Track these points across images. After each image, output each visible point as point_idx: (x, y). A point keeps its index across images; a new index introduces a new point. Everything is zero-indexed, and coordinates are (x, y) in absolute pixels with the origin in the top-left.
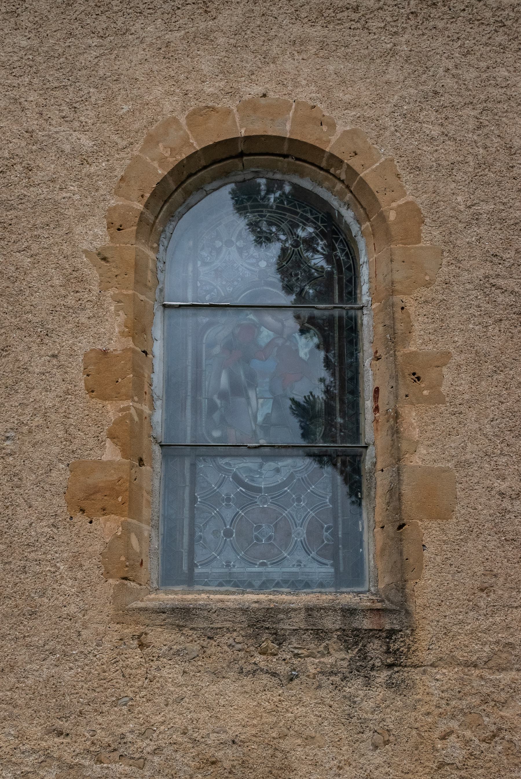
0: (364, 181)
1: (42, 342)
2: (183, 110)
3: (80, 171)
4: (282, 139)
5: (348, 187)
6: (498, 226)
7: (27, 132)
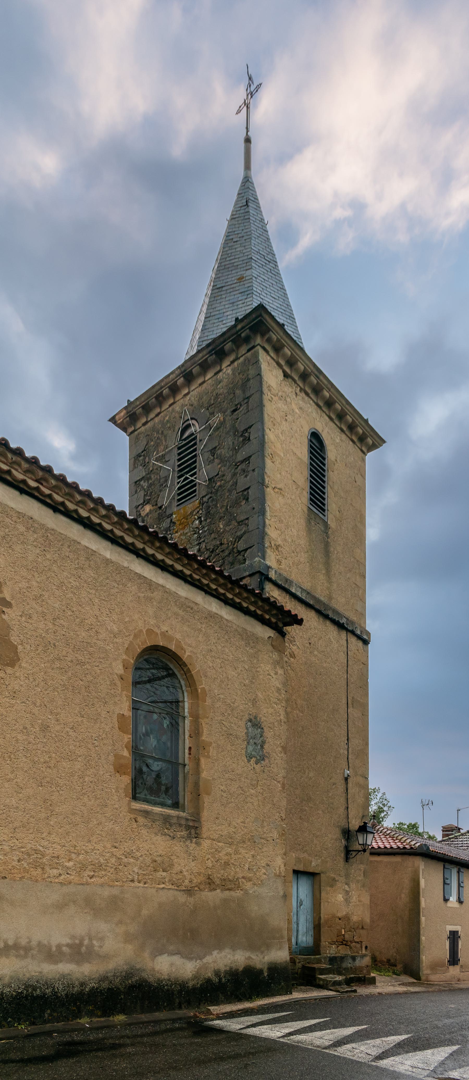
4: (171, 650)
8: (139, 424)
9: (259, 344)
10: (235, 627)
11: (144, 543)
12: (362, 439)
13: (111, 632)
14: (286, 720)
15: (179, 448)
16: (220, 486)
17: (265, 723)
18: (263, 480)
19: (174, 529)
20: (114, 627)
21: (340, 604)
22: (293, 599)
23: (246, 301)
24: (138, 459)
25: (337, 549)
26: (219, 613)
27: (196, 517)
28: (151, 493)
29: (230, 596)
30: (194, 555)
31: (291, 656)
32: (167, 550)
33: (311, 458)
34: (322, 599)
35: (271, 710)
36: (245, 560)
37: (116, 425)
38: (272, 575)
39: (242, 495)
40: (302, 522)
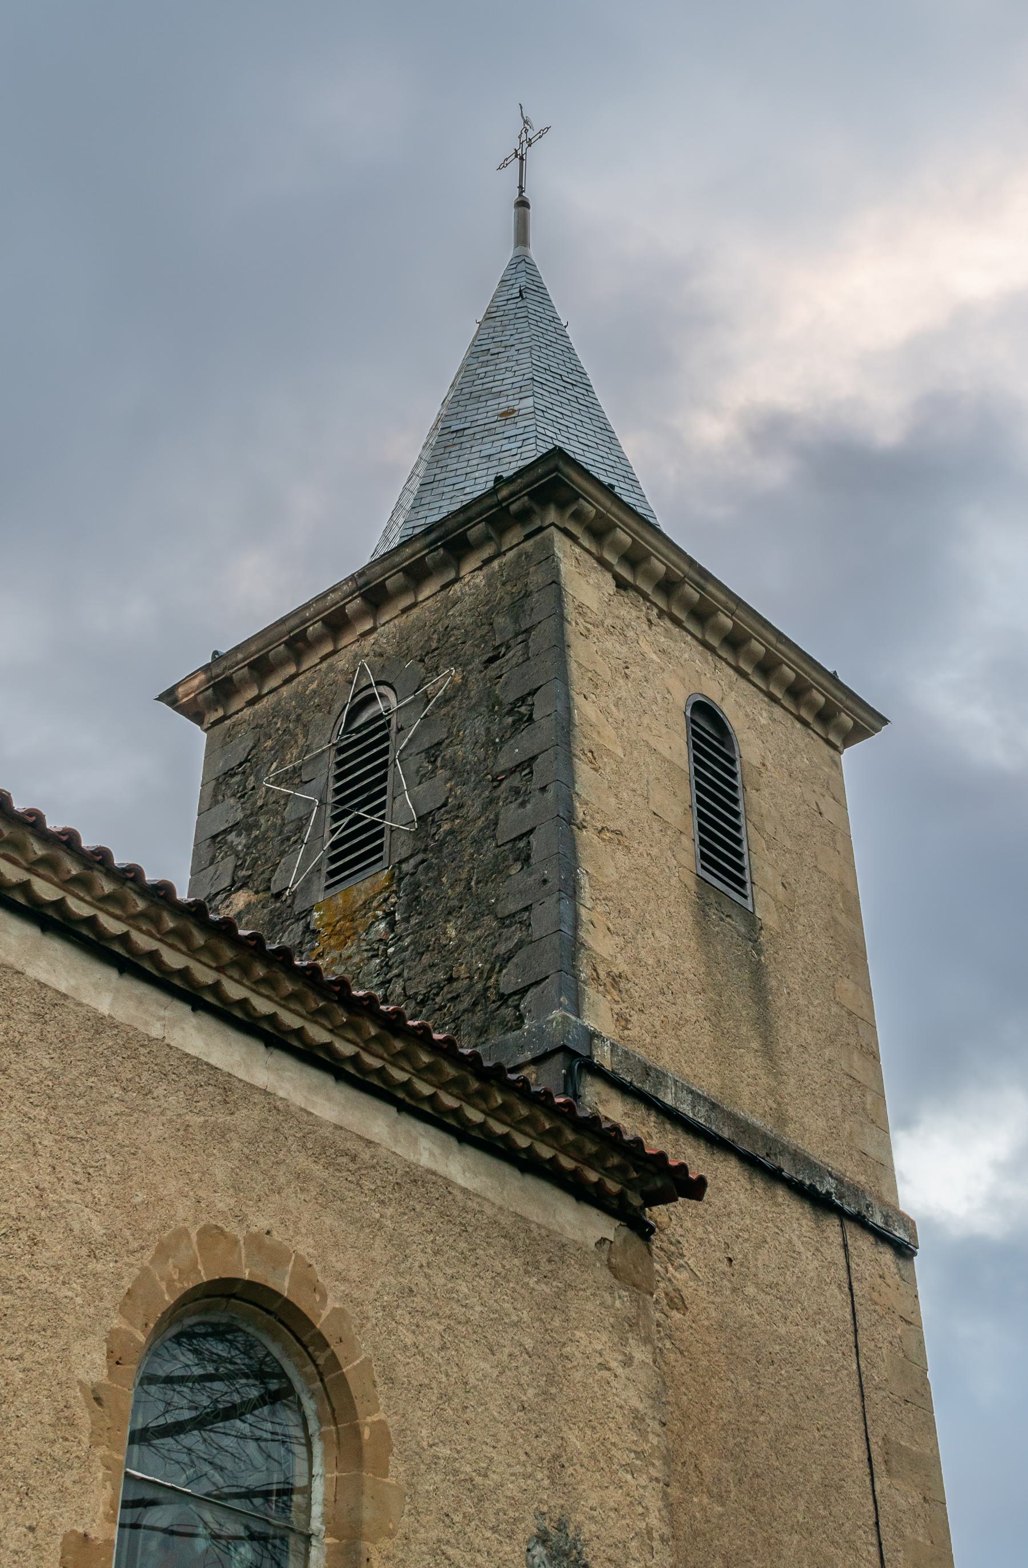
0: (345, 1379)
1: (20, 1505)
2: (196, 1223)
3: (86, 1265)
4: (277, 1295)
5: (320, 1374)
6: (452, 1479)
7: (37, 1187)
8: (237, 703)
9: (553, 524)
10: (489, 1211)
11: (219, 969)
12: (825, 716)
13: (85, 1239)
14: (666, 1531)
15: (340, 751)
16: (451, 832)
17: (595, 1544)
18: (571, 810)
19: (313, 949)
20: (95, 1225)
21: (810, 1133)
22: (668, 1126)
23: (520, 451)
24: (224, 782)
25: (789, 981)
26: (441, 1169)
27: (380, 913)
28: (255, 860)
29: (475, 1116)
30: (370, 998)
31: (672, 1305)
32: (289, 986)
33: (697, 760)
34: (757, 1122)
35: (615, 1496)
36: (521, 1018)
37: (176, 709)
38: (603, 1056)
39: (511, 850)
40: (685, 915)
